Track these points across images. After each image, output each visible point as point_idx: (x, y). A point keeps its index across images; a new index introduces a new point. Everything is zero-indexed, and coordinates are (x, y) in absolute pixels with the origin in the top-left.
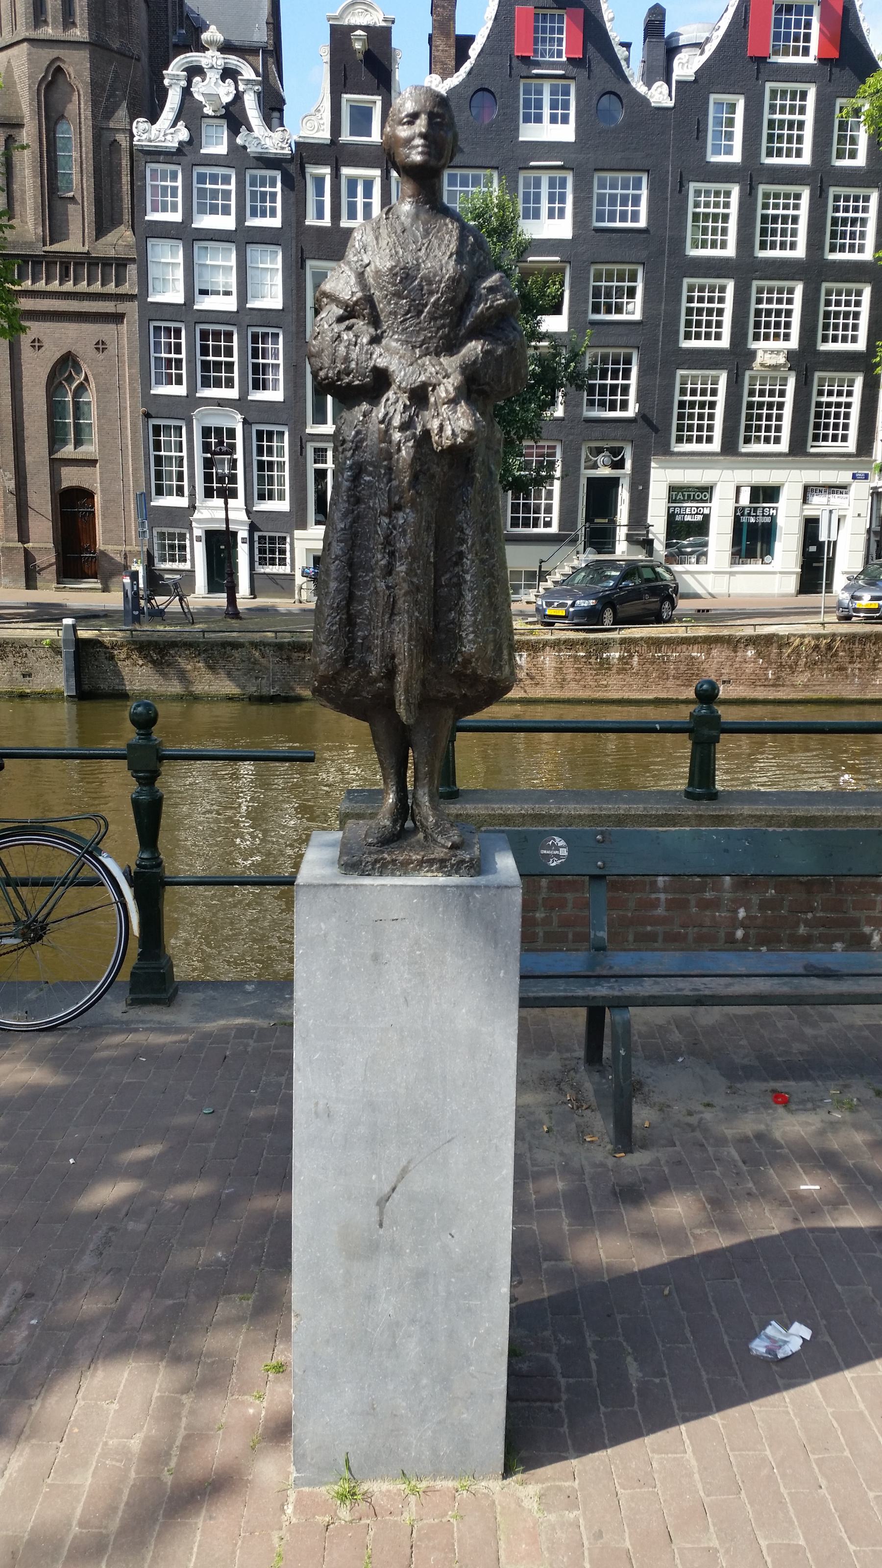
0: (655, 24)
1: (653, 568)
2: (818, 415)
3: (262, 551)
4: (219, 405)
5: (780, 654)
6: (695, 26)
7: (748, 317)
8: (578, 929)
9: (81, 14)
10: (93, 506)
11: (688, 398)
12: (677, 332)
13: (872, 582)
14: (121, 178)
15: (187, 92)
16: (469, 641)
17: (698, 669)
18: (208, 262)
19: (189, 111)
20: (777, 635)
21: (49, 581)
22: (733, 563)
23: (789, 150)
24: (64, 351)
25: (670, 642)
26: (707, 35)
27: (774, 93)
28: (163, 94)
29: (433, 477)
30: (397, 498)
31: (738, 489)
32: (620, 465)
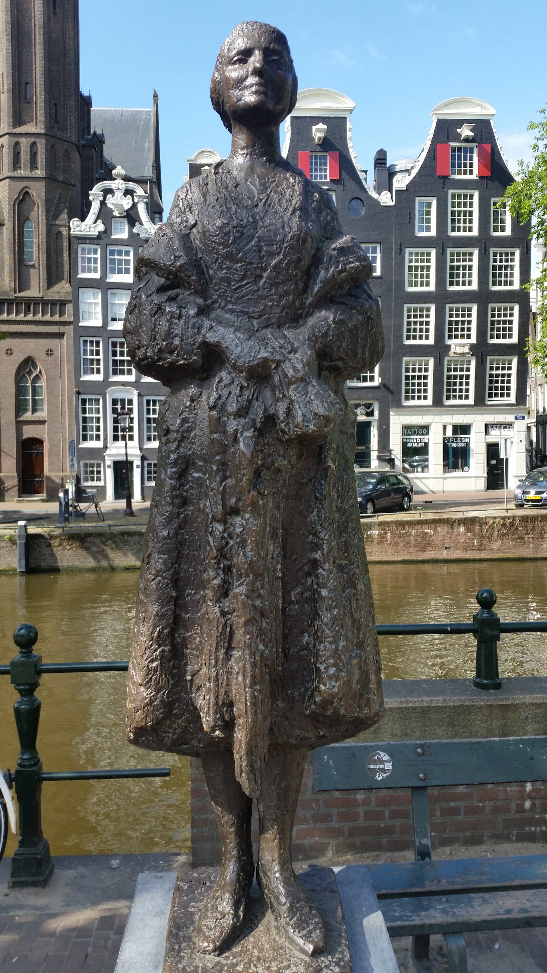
0: (380, 160)
1: (396, 477)
2: (491, 382)
3: (149, 472)
4: (123, 385)
5: (481, 530)
6: (404, 161)
7: (444, 325)
8: (393, 808)
9: (41, 162)
10: (43, 449)
11: (452, 373)
12: (402, 336)
13: (534, 483)
14: (63, 253)
15: (103, 203)
16: (330, 678)
17: (429, 540)
18: (117, 302)
19: (105, 214)
20: (478, 518)
21: (14, 496)
22: (445, 471)
23: (465, 228)
24: (26, 356)
25: (410, 523)
26: (412, 165)
27: (453, 196)
28: (89, 205)
29: (278, 471)
30: (233, 500)
31: (445, 427)
32: (371, 414)
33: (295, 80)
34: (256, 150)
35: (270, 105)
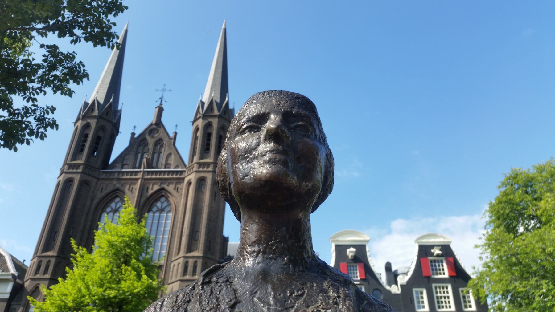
0: (388, 267)
33: (329, 157)
34: (272, 245)
35: (293, 180)
